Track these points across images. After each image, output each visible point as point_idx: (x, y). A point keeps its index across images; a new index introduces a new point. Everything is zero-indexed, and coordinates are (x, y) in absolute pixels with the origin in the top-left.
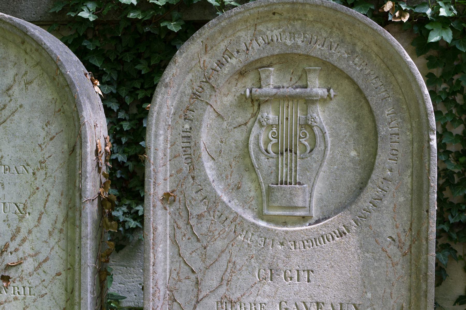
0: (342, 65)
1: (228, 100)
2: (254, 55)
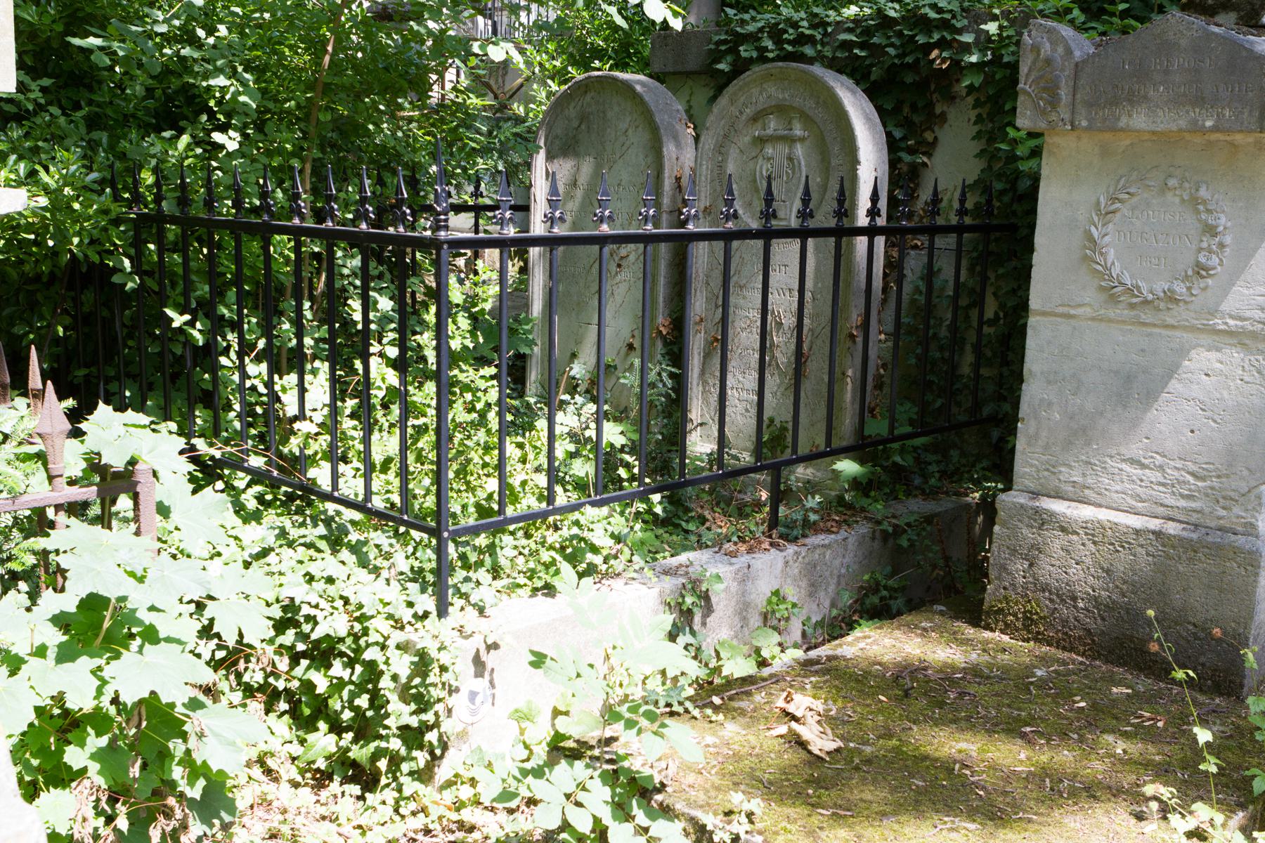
0: (811, 113)
1: (747, 139)
2: (760, 107)
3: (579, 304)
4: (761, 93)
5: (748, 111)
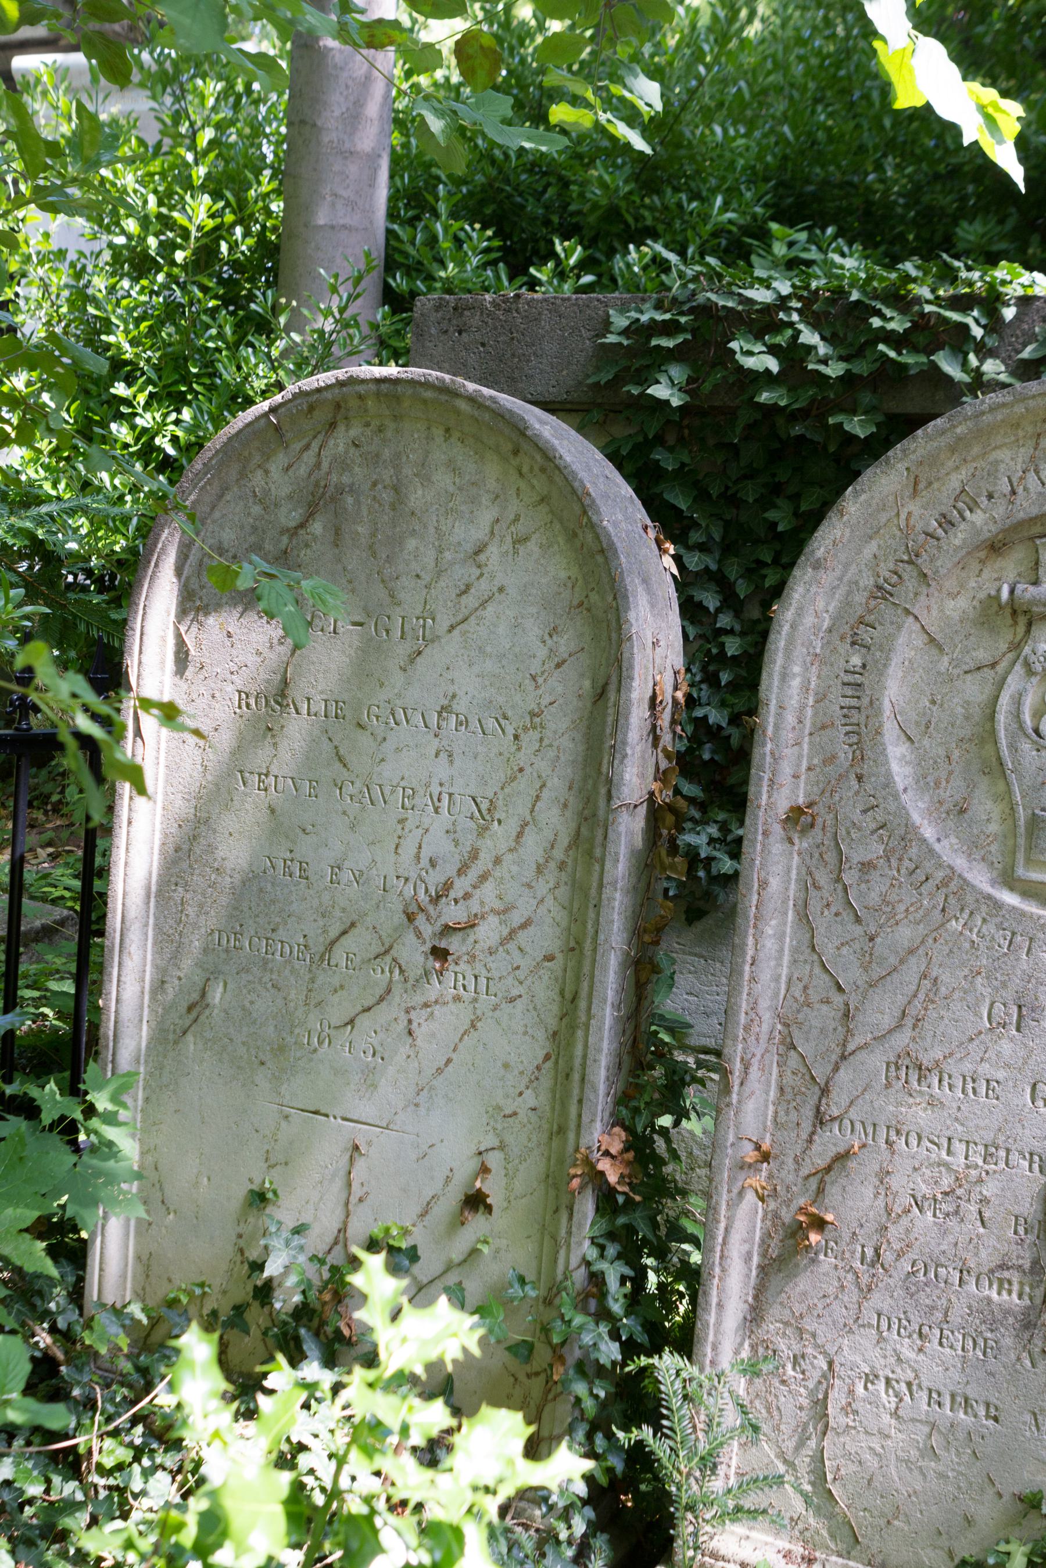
1: (958, 606)
3: (281, 1049)
5: (977, 518)
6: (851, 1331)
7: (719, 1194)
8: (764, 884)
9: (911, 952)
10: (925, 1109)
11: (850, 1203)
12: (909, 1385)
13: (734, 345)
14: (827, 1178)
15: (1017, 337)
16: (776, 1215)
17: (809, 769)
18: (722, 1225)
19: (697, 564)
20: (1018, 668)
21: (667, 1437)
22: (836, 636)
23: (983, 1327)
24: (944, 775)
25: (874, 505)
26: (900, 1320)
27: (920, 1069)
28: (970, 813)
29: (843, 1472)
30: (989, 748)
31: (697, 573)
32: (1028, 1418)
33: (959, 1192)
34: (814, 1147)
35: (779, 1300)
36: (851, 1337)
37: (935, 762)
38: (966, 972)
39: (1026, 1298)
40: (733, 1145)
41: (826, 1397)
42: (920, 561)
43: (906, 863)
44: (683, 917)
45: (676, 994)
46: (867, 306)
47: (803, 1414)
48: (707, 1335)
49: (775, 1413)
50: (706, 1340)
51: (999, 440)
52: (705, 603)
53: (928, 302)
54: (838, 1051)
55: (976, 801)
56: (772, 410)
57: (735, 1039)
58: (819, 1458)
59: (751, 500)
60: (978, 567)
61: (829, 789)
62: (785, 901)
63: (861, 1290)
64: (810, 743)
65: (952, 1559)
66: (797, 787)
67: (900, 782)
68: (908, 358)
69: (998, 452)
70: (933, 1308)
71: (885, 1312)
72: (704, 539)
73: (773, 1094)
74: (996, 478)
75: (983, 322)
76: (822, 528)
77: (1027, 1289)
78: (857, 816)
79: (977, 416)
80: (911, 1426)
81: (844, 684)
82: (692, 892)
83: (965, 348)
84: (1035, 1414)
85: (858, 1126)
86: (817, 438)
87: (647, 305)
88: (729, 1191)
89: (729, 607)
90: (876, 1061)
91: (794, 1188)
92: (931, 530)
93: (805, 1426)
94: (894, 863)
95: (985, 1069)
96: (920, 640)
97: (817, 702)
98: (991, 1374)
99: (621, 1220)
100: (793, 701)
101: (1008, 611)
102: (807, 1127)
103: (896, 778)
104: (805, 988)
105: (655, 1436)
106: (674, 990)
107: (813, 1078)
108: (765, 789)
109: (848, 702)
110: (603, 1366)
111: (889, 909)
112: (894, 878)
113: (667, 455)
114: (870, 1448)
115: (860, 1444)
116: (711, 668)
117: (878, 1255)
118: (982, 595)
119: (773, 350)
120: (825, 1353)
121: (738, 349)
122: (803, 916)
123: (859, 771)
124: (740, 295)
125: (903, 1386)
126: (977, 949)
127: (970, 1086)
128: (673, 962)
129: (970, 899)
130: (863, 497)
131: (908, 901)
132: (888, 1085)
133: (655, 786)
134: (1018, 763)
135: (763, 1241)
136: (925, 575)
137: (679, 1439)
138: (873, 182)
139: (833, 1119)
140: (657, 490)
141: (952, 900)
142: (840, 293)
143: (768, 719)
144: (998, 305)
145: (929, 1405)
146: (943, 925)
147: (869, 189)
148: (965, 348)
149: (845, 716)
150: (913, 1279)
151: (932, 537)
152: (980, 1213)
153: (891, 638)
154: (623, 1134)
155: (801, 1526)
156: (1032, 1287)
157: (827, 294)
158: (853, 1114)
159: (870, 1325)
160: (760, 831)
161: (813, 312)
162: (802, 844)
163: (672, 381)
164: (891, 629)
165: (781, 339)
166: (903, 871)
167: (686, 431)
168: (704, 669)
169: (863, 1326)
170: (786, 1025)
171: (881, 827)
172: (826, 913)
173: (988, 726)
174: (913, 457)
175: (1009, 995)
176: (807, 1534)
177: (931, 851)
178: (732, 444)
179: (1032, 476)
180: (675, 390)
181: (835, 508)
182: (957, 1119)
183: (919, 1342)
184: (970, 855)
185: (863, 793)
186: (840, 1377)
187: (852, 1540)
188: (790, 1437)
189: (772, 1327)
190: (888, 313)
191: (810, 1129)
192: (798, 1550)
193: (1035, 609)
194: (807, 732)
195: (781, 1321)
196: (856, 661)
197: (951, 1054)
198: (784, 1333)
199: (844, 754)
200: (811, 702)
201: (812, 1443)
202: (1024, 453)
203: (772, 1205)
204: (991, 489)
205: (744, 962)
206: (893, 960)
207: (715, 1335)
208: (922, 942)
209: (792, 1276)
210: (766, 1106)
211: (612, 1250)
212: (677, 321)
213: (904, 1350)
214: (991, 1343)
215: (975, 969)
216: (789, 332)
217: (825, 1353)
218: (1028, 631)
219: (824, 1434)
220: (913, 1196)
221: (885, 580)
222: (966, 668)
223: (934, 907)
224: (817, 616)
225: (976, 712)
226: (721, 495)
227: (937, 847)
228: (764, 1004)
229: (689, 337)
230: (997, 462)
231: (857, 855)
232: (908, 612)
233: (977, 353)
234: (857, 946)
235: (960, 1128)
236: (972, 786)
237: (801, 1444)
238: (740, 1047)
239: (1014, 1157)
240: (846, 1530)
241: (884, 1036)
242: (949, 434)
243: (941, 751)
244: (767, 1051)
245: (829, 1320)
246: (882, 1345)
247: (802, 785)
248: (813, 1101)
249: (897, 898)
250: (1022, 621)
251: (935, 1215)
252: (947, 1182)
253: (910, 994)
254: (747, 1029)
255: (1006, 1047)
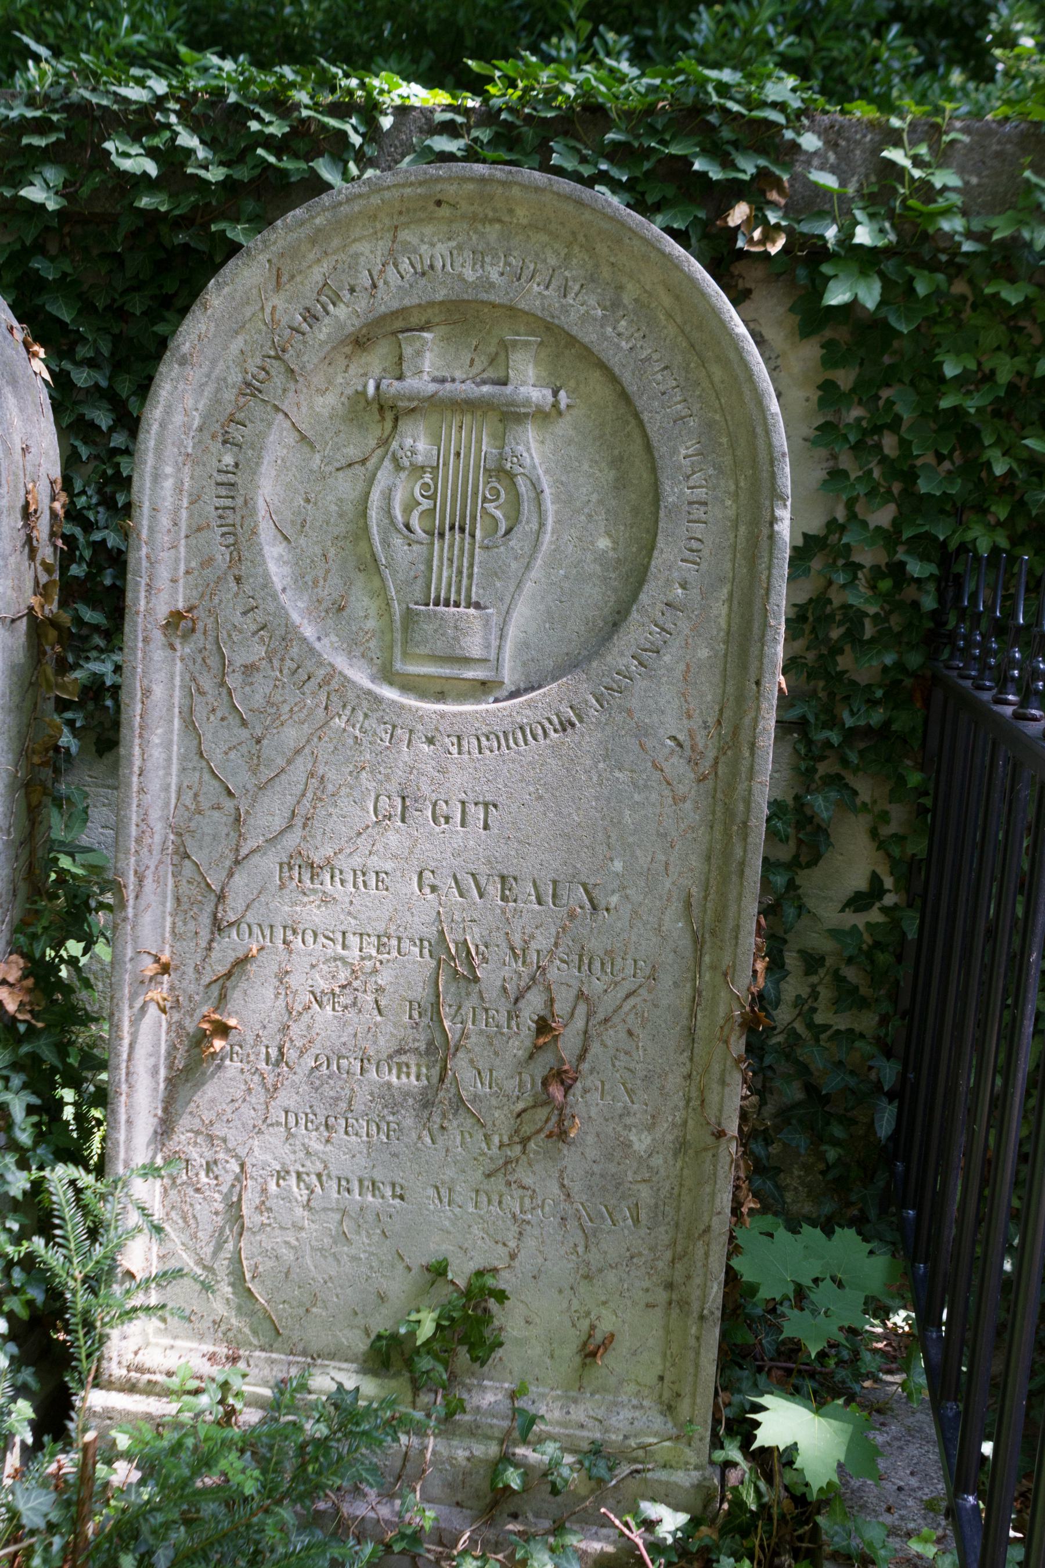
0: (589, 336)
1: (327, 403)
2: (387, 301)
4: (392, 258)
5: (341, 312)
6: (260, 1132)
7: (121, 1011)
8: (147, 692)
9: (298, 752)
10: (319, 906)
11: (253, 1006)
12: (319, 1176)
13: (109, 145)
14: (228, 984)
15: (396, 147)
16: (180, 1026)
17: (187, 572)
18: (126, 1042)
19: (86, 380)
20: (387, 463)
21: (61, 1245)
22: (206, 435)
23: (386, 1111)
24: (321, 574)
25: (238, 298)
26: (306, 1115)
27: (312, 867)
28: (348, 610)
29: (261, 1269)
30: (363, 544)
31: (87, 390)
32: (431, 1192)
33: (356, 984)
34: (213, 954)
35: (188, 1110)
36: (261, 1137)
37: (312, 561)
38: (351, 768)
39: (424, 1078)
40: (132, 959)
41: (240, 1199)
42: (286, 356)
43: (288, 663)
44: (94, 749)
45: (90, 829)
46: (246, 110)
47: (219, 1218)
48: (118, 1153)
49: (192, 1221)
50: (117, 1159)
51: (357, 232)
52: (97, 422)
53: (306, 107)
54: (232, 856)
55: (353, 598)
56: (152, 217)
57: (127, 852)
58: (237, 1259)
59: (138, 313)
60: (345, 362)
61: (209, 591)
62: (170, 709)
63: (267, 1090)
64: (187, 545)
65: (368, 1335)
66: (176, 592)
67: (278, 584)
68: (288, 164)
69: (357, 244)
70: (337, 1099)
71: (292, 1108)
72: (91, 354)
73: (170, 905)
74: (357, 271)
75: (362, 130)
76: (186, 322)
77: (424, 1070)
78: (237, 619)
79: (334, 207)
80: (323, 1215)
81: (218, 484)
82: (101, 723)
83: (345, 156)
84: (437, 1188)
85: (256, 930)
86: (202, 247)
87: (18, 102)
88: (131, 1007)
89: (123, 426)
90: (269, 863)
91: (197, 998)
92: (296, 325)
93: (222, 1229)
94: (276, 663)
95: (374, 862)
96: (291, 438)
97: (191, 503)
98: (395, 1155)
99: (25, 1049)
100: (168, 504)
101: (375, 406)
102: (205, 934)
103: (274, 579)
104: (196, 795)
105: (47, 1245)
106: (89, 824)
107: (208, 885)
108: (143, 594)
109: (223, 502)
110: (14, 1198)
111: (273, 711)
112: (277, 679)
113: (47, 264)
114: (286, 1243)
115: (276, 1240)
116: (108, 490)
117: (282, 1054)
118: (349, 391)
119: (152, 153)
120: (237, 1157)
121: (113, 150)
122: (189, 724)
123: (237, 573)
124: (115, 94)
125: (314, 1178)
126: (360, 745)
127: (360, 880)
128: (86, 796)
129: (351, 695)
130: (226, 290)
131: (292, 701)
132: (282, 887)
133: (34, 601)
134: (390, 558)
135: (169, 1054)
136: (292, 371)
137: (72, 1246)
138: (291, 15)
139: (231, 925)
140: (39, 301)
141: (334, 698)
142: (219, 93)
143: (143, 520)
144: (376, 113)
145: (339, 1192)
146: (327, 723)
147: (286, 22)
148: (345, 156)
149: (220, 517)
150: (317, 1073)
151: (298, 332)
152: (377, 1002)
153: (262, 435)
154: (21, 962)
155: (223, 1327)
156: (428, 1068)
157: (206, 96)
158: (250, 918)
159: (278, 1124)
160: (140, 638)
161: (193, 115)
162: (185, 649)
163: (48, 185)
164: (261, 426)
165: (157, 142)
166: (285, 672)
167: (68, 240)
168: (100, 491)
169: (272, 1125)
170: (179, 835)
171: (262, 629)
172: (212, 718)
173: (361, 523)
174: (273, 248)
175: (393, 787)
176: (230, 1334)
177: (312, 650)
178: (116, 254)
179: (391, 269)
180: (52, 194)
181: (198, 302)
182: (349, 913)
183: (326, 1134)
184: (350, 652)
185: (242, 595)
186: (252, 1178)
187: (273, 1332)
188: (208, 1243)
189: (183, 1137)
190: (267, 117)
191: (208, 937)
192: (222, 1350)
193: (400, 404)
194: (183, 534)
195: (191, 1131)
196: (228, 460)
197: (341, 850)
198: (196, 1143)
199: (221, 556)
200: (185, 505)
201: (230, 1246)
202: (383, 245)
203: (176, 1017)
204: (352, 283)
205: (131, 773)
206: (281, 762)
207: (127, 1151)
208: (308, 741)
209: (200, 1084)
210: (164, 918)
211: (17, 1081)
212: (50, 119)
213: (312, 1143)
214: (393, 1126)
215: (359, 765)
216: (167, 134)
217: (237, 1157)
218: (395, 427)
219: (241, 1235)
220: (312, 992)
221: (254, 377)
222: (338, 465)
223: (317, 706)
224: (186, 415)
225: (349, 508)
226: (107, 308)
227: (317, 646)
228: (155, 814)
229: (63, 136)
230: (356, 256)
231: (240, 658)
232: (277, 409)
233: (357, 162)
234: (244, 749)
235: (353, 921)
236: (349, 583)
237: (219, 1248)
238: (133, 859)
239: (406, 944)
240: (267, 1325)
241: (275, 837)
242: (308, 225)
243: (318, 550)
244: (161, 862)
245: (238, 1124)
246: (291, 1141)
247: (181, 590)
248: (209, 908)
249: (281, 699)
250: (389, 416)
251: (334, 1009)
252: (343, 975)
253: (299, 793)
254: (139, 841)
255: (393, 839)
